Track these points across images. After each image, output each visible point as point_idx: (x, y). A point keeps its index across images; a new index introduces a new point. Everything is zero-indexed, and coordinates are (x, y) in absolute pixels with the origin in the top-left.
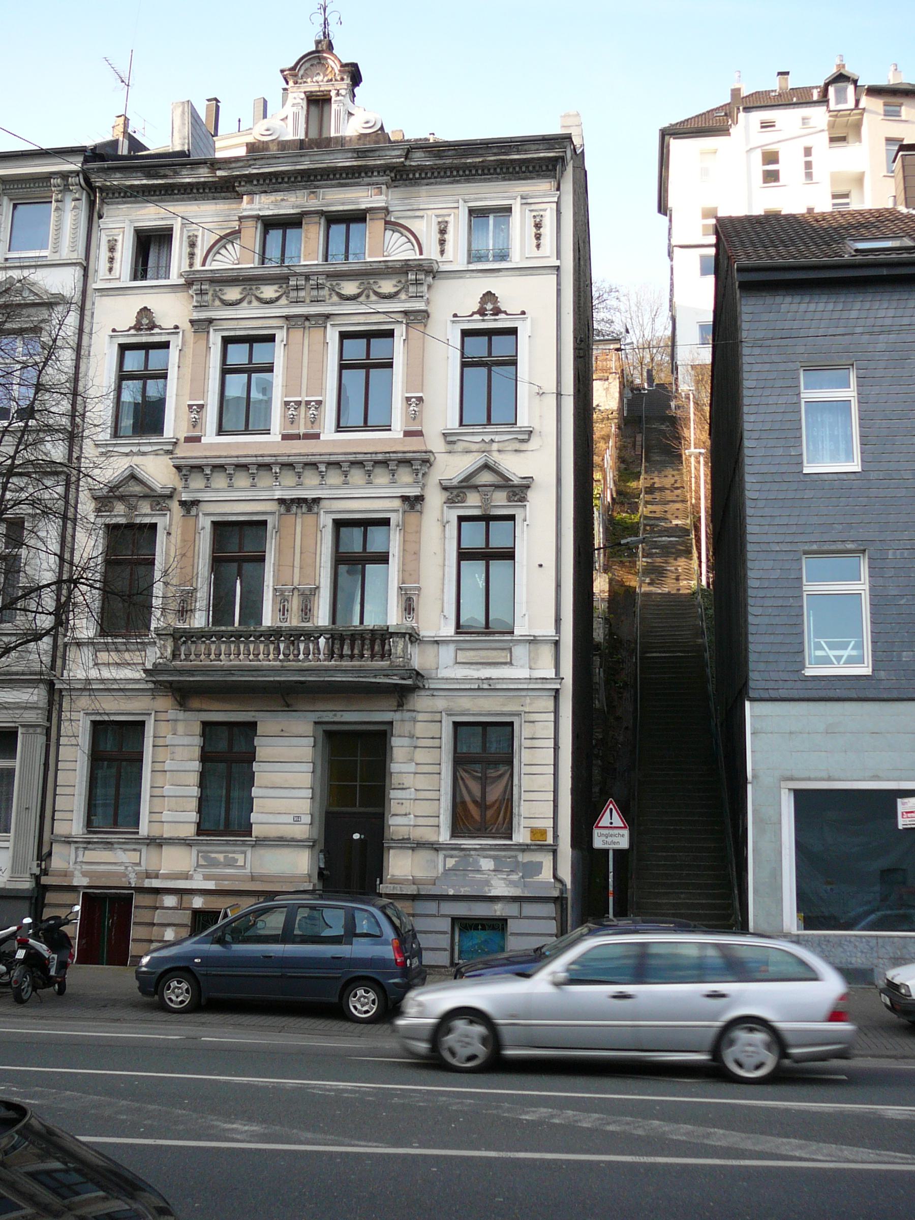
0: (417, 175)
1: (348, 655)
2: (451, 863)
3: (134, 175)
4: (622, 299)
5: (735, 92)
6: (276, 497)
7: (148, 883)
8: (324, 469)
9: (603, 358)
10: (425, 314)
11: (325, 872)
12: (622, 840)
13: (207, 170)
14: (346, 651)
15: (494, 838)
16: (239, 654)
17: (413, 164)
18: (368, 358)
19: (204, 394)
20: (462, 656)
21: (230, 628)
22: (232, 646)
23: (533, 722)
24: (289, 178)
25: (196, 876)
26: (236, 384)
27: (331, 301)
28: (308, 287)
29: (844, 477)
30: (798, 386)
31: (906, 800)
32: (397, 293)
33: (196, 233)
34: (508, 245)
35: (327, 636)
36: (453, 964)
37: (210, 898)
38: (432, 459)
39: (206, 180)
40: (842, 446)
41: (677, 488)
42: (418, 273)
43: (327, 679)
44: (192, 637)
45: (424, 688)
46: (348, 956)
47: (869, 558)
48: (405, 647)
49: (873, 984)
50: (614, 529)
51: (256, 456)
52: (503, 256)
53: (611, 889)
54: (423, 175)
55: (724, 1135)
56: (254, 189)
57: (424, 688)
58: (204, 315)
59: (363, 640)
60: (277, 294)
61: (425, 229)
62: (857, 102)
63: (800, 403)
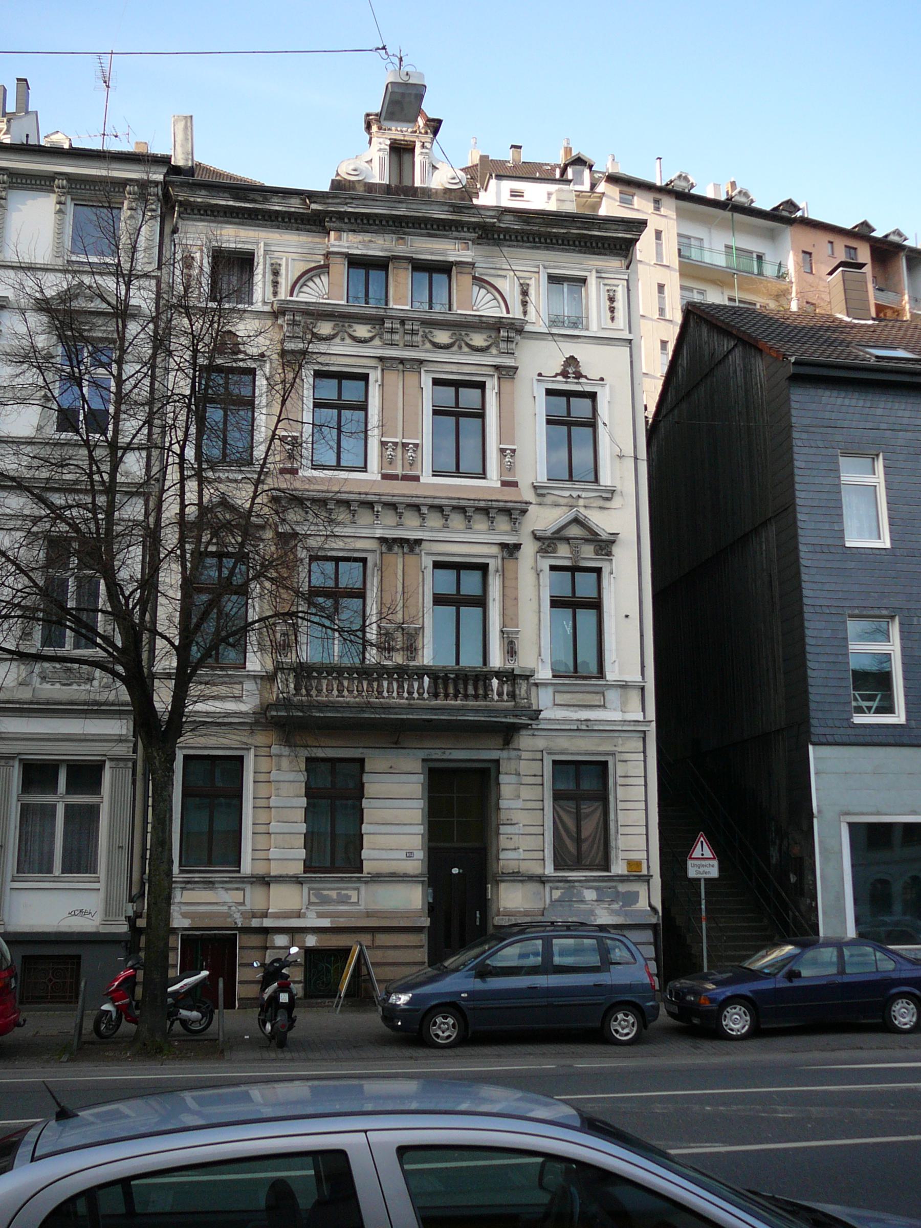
0: (502, 237)
2: (557, 894)
3: (221, 195)
6: (378, 536)
7: (255, 923)
12: (712, 870)
13: (298, 201)
14: (471, 690)
20: (560, 698)
23: (626, 761)
32: (488, 347)
33: (279, 262)
39: (297, 210)
42: (506, 331)
54: (507, 237)
56: (343, 226)
60: (370, 335)
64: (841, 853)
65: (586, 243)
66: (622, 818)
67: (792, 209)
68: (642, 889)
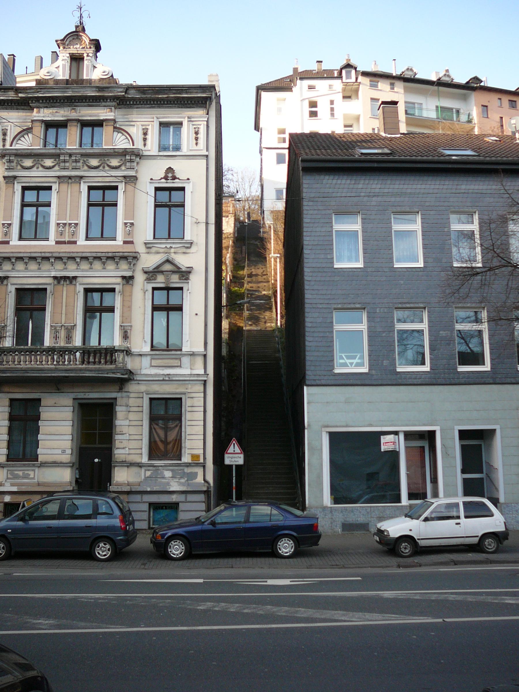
0: (131, 103)
1: (92, 362)
2: (148, 473)
4: (235, 175)
5: (295, 70)
6: (52, 276)
8: (79, 261)
9: (228, 206)
10: (135, 178)
11: (79, 480)
12: (240, 460)
13: (13, 93)
14: (91, 359)
15: (172, 460)
16: (31, 361)
17: (129, 96)
18: (104, 200)
19: (11, 217)
20: (154, 363)
21: (26, 347)
22: (27, 357)
23: (192, 398)
24: (60, 100)
25: (6, 484)
26: (29, 212)
27: (83, 169)
28: (71, 161)
29: (355, 270)
30: (332, 223)
31: (385, 436)
33: (7, 128)
34: (180, 142)
35: (81, 352)
36: (150, 528)
37: (15, 496)
38: (139, 256)
39: (13, 98)
40: (354, 254)
41: (265, 275)
42: (132, 156)
43: (81, 375)
44: (5, 352)
45: (134, 380)
46: (95, 525)
47: (367, 312)
48: (124, 357)
49: (368, 531)
50: (233, 297)
51: (41, 253)
52: (177, 148)
53: (234, 485)
54: (135, 103)
55: (304, 611)
57: (134, 380)
58: (11, 174)
59: (101, 354)
60: (53, 164)
61: (135, 132)
62: (357, 79)
63: (332, 231)
64: (322, 449)
65: (181, 102)
66: (189, 430)
67: (478, 82)
68: (200, 471)
